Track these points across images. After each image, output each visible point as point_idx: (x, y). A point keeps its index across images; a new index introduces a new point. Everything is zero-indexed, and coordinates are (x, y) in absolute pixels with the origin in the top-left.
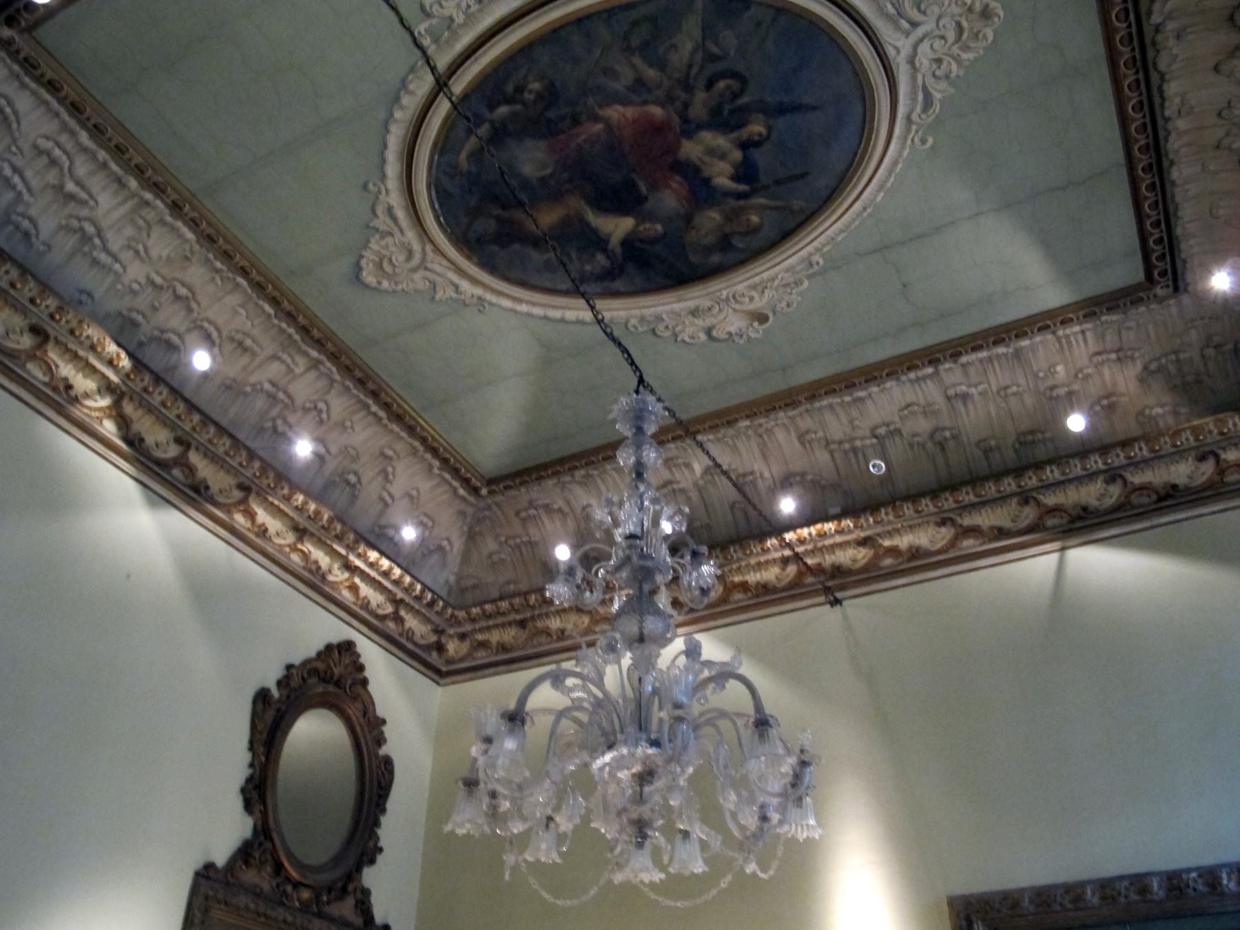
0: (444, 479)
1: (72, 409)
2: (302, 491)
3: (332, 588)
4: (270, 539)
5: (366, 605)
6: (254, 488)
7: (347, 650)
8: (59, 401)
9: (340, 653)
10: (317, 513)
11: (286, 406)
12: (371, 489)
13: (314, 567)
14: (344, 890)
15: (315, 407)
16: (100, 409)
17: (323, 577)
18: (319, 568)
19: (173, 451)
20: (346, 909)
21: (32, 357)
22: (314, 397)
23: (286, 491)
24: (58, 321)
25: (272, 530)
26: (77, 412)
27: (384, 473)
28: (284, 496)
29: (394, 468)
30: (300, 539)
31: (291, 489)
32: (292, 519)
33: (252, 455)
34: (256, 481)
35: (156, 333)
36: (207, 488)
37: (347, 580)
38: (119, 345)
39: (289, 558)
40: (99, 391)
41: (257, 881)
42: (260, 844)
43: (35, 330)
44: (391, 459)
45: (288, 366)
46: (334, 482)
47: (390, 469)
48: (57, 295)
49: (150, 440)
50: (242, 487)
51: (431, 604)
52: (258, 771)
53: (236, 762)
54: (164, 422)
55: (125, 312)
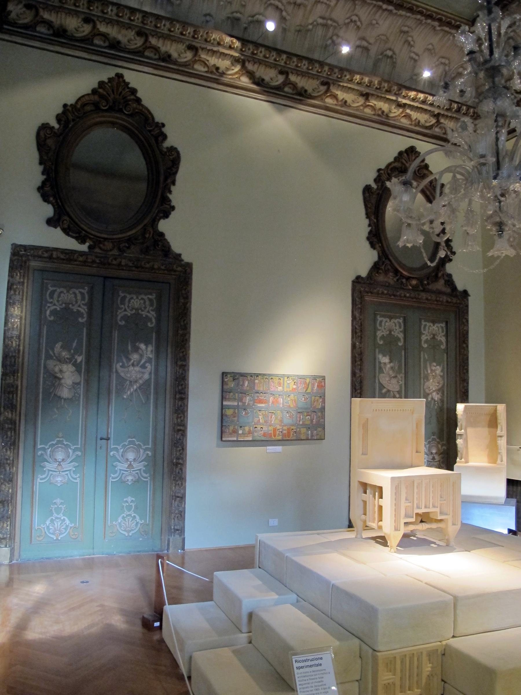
0: (446, 31)
1: (224, 79)
2: (358, 73)
3: (394, 120)
4: (350, 106)
5: (418, 124)
6: (330, 81)
7: (412, 152)
8: (215, 78)
9: (408, 155)
10: (370, 82)
11: (335, 28)
12: (402, 54)
13: (380, 112)
14: (436, 276)
15: (351, 21)
16: (236, 73)
17: (387, 116)
18: (383, 112)
19: (281, 79)
20: (440, 285)
21: (195, 62)
22: (348, 15)
23: (348, 77)
24: (197, 38)
25: (349, 101)
26: (225, 79)
27: (406, 41)
28: (348, 79)
29: (412, 37)
30: (367, 99)
31: (350, 74)
32: (358, 90)
33: (322, 64)
34: (330, 77)
35: (250, 19)
36: (306, 91)
37: (402, 113)
38: (231, 36)
39: (363, 112)
40: (233, 64)
41: (386, 280)
42: (383, 262)
43: (191, 48)
44: (408, 32)
45: (326, 4)
46: (379, 59)
47: (410, 39)
48: (192, 25)
49: (267, 78)
50: (323, 84)
51: (458, 110)
52: (374, 228)
53: (362, 226)
54: (269, 65)
55: (230, 15)
